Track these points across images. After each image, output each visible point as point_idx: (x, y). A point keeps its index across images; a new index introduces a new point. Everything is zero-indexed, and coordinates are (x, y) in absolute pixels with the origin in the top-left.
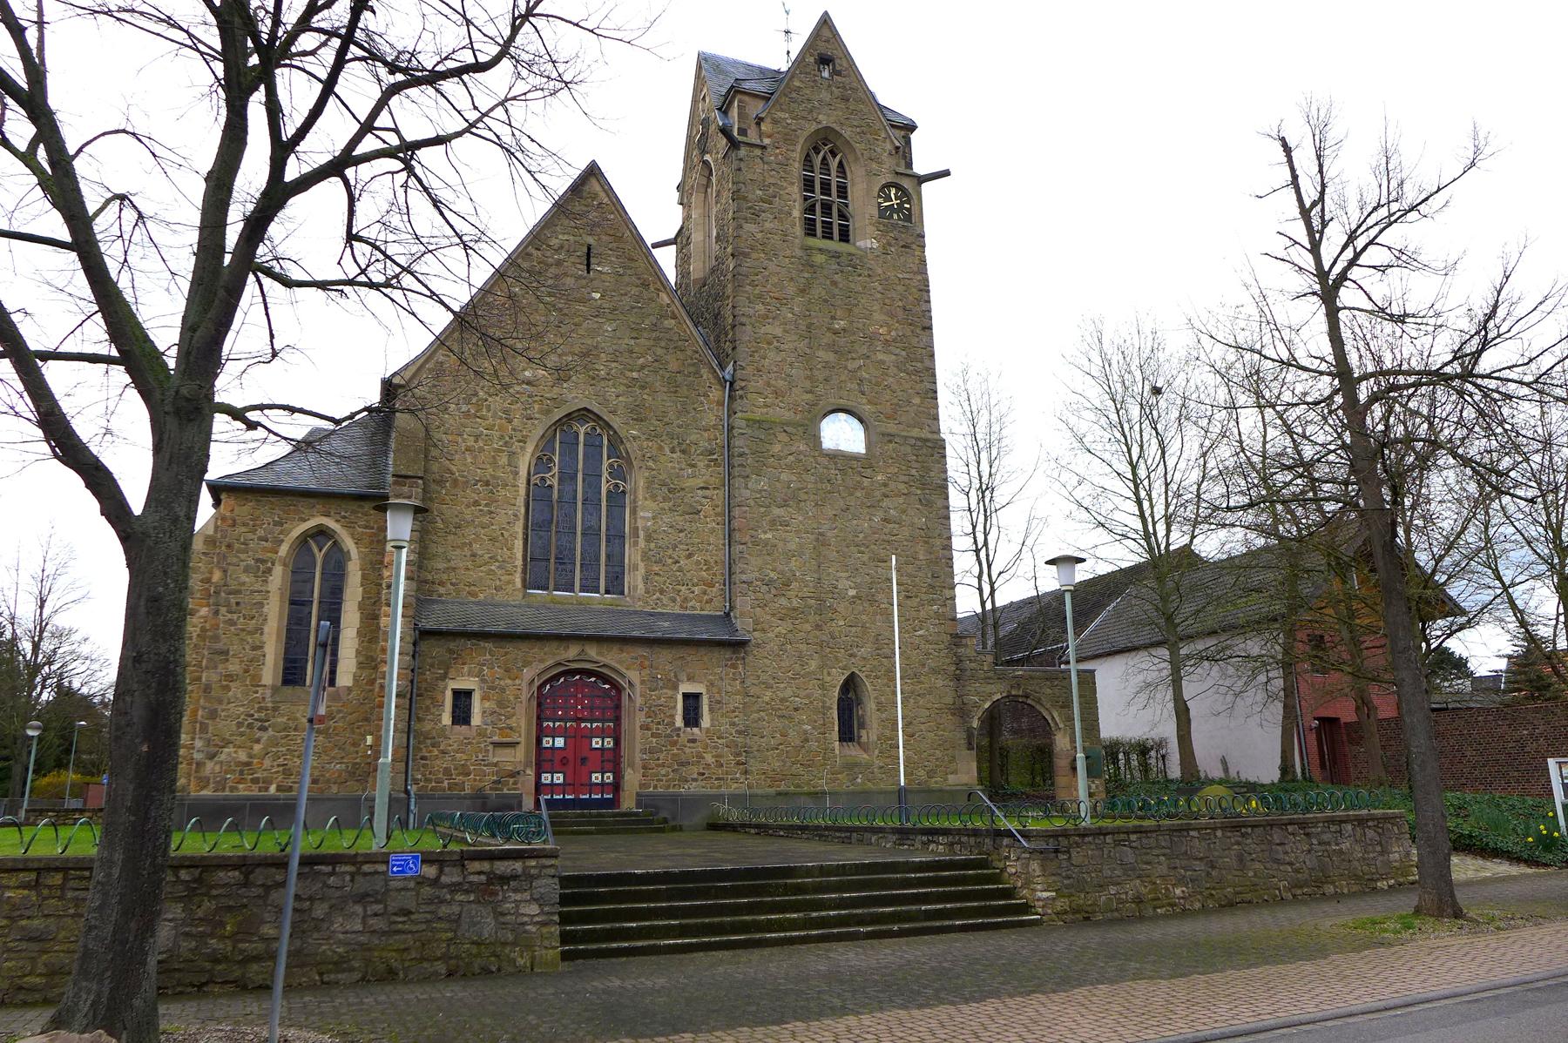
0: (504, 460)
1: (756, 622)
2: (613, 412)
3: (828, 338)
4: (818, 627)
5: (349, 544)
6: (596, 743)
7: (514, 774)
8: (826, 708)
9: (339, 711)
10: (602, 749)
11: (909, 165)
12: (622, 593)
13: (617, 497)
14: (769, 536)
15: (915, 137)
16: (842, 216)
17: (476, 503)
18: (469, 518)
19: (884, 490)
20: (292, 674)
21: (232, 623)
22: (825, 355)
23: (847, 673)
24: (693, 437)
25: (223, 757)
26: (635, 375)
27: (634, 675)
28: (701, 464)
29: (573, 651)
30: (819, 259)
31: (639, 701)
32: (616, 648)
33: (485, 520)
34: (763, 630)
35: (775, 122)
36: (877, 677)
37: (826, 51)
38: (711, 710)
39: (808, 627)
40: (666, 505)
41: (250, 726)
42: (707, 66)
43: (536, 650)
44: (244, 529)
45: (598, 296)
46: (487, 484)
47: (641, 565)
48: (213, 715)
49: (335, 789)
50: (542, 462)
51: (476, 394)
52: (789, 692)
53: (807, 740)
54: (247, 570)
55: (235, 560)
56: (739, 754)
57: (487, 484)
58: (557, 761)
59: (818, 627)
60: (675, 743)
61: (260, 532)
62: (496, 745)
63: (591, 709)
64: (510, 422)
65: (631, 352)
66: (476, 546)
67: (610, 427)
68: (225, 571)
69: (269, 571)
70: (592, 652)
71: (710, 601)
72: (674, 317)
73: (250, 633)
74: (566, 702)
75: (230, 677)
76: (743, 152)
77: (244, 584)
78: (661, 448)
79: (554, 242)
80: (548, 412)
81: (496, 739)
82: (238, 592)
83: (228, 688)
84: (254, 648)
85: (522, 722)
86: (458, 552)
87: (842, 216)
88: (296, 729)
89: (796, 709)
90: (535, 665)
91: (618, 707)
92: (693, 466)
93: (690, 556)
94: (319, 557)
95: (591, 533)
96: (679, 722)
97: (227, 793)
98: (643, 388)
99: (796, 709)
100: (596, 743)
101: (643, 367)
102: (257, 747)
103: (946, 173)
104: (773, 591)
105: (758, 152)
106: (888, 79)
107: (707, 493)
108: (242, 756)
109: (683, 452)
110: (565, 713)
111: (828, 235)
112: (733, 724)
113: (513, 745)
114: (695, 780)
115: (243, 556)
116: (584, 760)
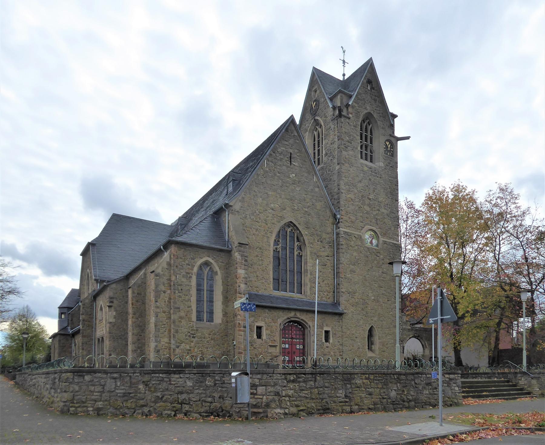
0: (266, 240)
3: (367, 201)
5: (216, 268)
6: (298, 347)
7: (276, 357)
9: (218, 332)
10: (300, 349)
11: (393, 133)
16: (371, 152)
17: (257, 256)
18: (255, 261)
19: (383, 261)
21: (180, 297)
22: (367, 208)
24: (324, 237)
25: (182, 347)
26: (306, 210)
28: (326, 247)
29: (292, 314)
32: (305, 313)
33: (261, 263)
41: (189, 336)
42: (292, 115)
43: (281, 313)
44: (181, 260)
47: (309, 283)
48: (177, 332)
50: (276, 242)
53: (359, 348)
54: (183, 276)
55: (179, 272)
56: (340, 352)
57: (260, 249)
58: (286, 352)
60: (322, 348)
62: (271, 346)
67: (298, 229)
69: (191, 277)
70: (298, 314)
71: (329, 298)
72: (318, 187)
73: (186, 301)
75: (181, 318)
76: (343, 119)
77: (183, 282)
78: (314, 240)
79: (279, 150)
81: (270, 344)
82: (181, 285)
84: (189, 307)
85: (277, 338)
86: (252, 275)
87: (371, 152)
88: (204, 338)
90: (282, 318)
91: (304, 335)
92: (324, 247)
93: (323, 281)
96: (324, 341)
98: (309, 215)
99: (356, 338)
100: (298, 347)
101: (309, 207)
102: (192, 344)
103: (408, 138)
107: (328, 258)
109: (321, 242)
111: (366, 159)
112: (339, 342)
113: (275, 346)
115: (182, 271)
116: (294, 352)
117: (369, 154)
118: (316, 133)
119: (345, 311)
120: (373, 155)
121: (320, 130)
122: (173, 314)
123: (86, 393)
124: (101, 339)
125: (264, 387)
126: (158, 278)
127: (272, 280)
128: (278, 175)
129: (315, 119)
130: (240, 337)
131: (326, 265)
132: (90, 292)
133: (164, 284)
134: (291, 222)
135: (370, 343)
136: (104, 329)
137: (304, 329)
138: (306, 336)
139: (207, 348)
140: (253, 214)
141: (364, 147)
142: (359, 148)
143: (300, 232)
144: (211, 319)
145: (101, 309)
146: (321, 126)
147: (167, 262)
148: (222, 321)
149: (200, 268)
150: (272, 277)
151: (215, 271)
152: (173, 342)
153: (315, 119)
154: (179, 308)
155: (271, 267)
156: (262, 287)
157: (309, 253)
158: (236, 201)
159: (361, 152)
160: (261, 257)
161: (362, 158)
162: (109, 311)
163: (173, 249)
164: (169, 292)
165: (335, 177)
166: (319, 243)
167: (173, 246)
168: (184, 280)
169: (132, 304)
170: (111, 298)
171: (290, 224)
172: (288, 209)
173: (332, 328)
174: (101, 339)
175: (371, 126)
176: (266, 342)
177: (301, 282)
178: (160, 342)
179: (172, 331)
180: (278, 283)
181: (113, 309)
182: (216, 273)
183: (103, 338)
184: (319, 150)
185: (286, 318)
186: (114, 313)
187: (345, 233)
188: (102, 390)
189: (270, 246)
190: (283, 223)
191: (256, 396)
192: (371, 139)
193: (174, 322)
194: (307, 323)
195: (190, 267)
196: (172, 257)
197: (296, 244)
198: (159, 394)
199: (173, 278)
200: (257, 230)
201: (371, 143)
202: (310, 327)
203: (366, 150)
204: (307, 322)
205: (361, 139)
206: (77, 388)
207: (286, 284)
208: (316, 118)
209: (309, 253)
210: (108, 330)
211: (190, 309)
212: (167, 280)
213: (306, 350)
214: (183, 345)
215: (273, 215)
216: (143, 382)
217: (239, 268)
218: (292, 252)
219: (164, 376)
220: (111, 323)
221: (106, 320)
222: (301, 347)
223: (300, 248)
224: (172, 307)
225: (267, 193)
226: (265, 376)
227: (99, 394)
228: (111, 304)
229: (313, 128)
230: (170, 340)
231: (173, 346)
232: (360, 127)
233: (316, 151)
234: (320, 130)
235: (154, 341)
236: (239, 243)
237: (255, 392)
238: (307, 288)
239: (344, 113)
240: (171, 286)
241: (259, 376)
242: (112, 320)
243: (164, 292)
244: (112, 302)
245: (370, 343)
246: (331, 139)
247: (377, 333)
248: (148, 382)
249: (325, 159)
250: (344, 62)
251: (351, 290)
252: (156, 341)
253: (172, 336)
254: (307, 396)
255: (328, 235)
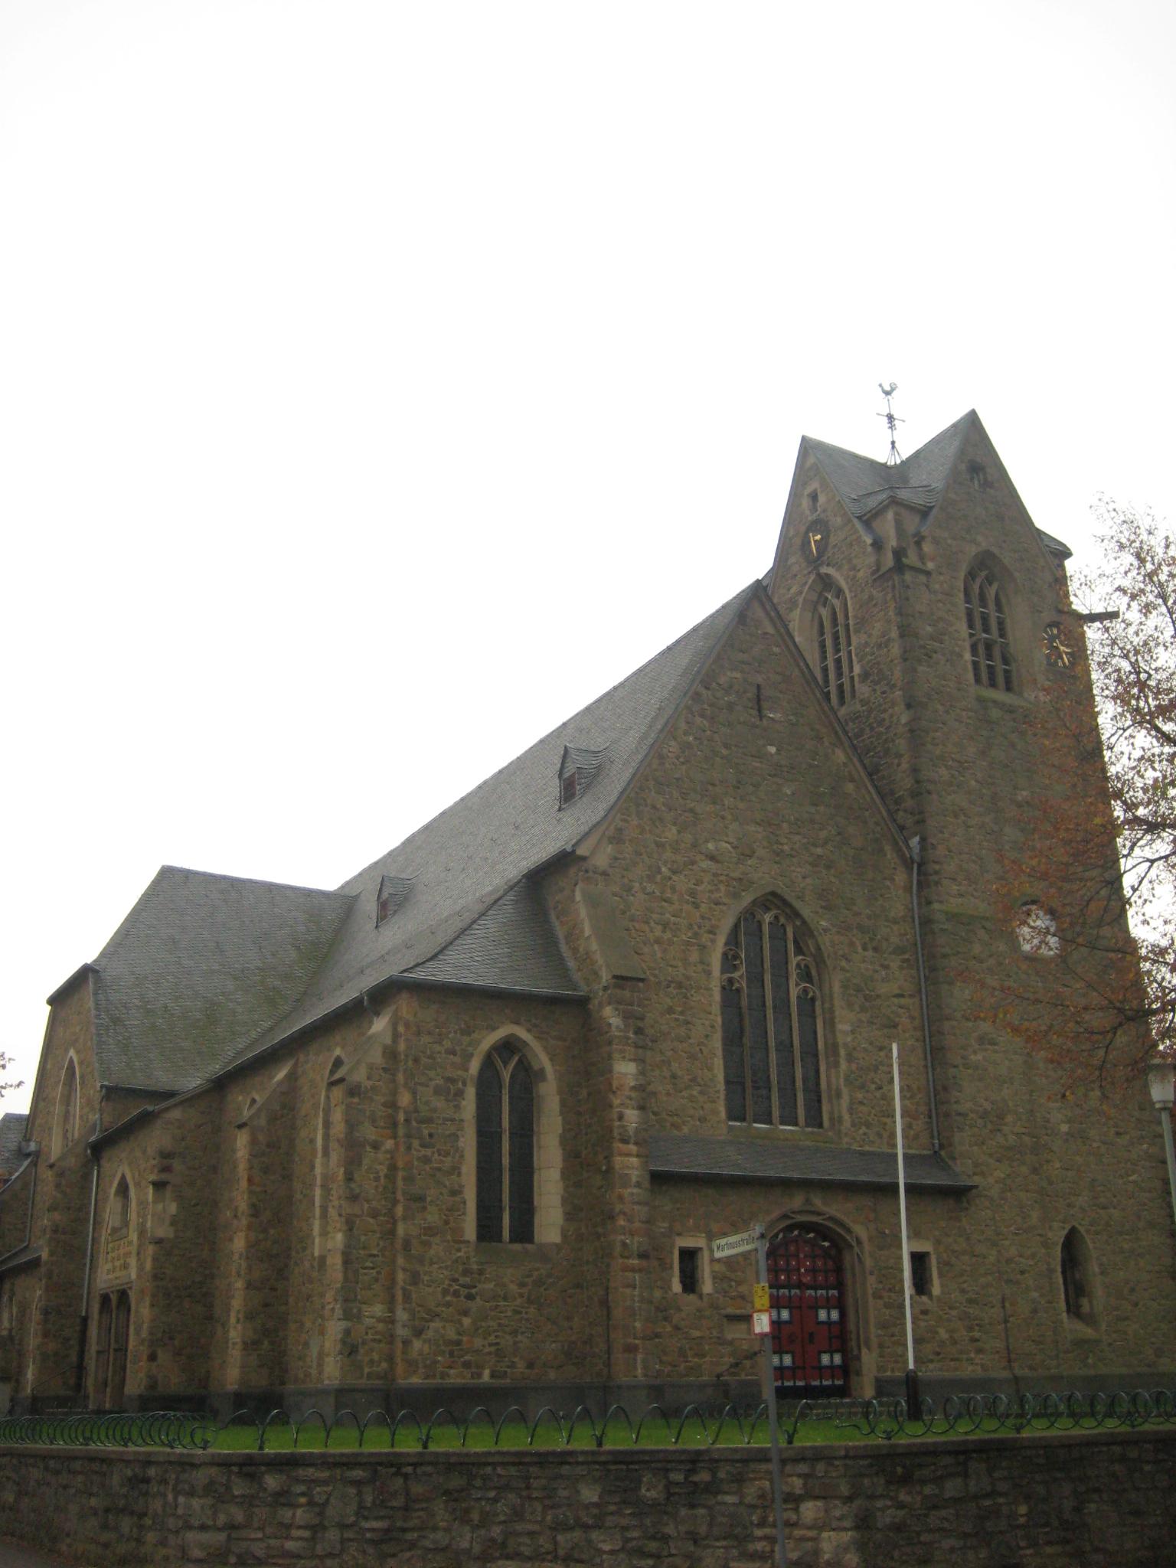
0: (694, 956)
1: (976, 1165)
2: (800, 898)
4: (1035, 1171)
5: (542, 1059)
6: (822, 1315)
8: (1051, 1271)
12: (820, 1125)
13: (808, 1003)
14: (979, 1057)
15: (1069, 565)
16: (1006, 661)
17: (670, 1010)
20: (488, 1230)
21: (426, 1160)
23: (1068, 1227)
25: (430, 1334)
26: (819, 851)
27: (860, 1231)
29: (797, 1201)
30: (995, 713)
31: (869, 1263)
33: (682, 1031)
34: (983, 1174)
35: (936, 541)
36: (1097, 1233)
37: (969, 451)
38: (941, 1275)
39: (1024, 1170)
40: (864, 1017)
41: (456, 1294)
45: (772, 750)
46: (680, 985)
48: (415, 1279)
49: (552, 1375)
50: (729, 961)
51: (660, 872)
52: (1013, 1251)
54: (437, 1091)
56: (970, 1329)
57: (680, 985)
59: (1035, 1171)
61: (447, 1044)
63: (813, 1271)
64: (696, 906)
65: (812, 821)
66: (675, 1065)
68: (414, 1093)
69: (460, 1094)
70: (818, 1202)
72: (852, 780)
74: (788, 1263)
75: (430, 1231)
76: (908, 577)
77: (435, 1110)
80: (736, 896)
81: (730, 1311)
82: (429, 1120)
83: (427, 1244)
88: (505, 1299)
89: (1022, 1273)
91: (839, 1270)
92: (886, 967)
94: (506, 1075)
95: (785, 1047)
97: (889, 1374)
98: (828, 867)
99: (1022, 1273)
102: (467, 1321)
104: (990, 1126)
105: (923, 578)
106: (1053, 498)
107: (903, 1001)
108: (451, 1333)
109: (875, 949)
110: (788, 1277)
111: (993, 684)
112: (963, 1291)
114: (931, 1361)
115: (432, 1074)
117: (1000, 667)
118: (824, 612)
119: (977, 1180)
120: (1013, 667)
121: (836, 603)
122: (404, 1218)
123: (268, 1530)
124: (114, 1298)
125: (819, 1504)
126: (356, 1100)
127: (721, 1087)
128: (725, 752)
129: (819, 575)
130: (628, 1291)
131: (895, 1026)
132: (76, 1129)
133: (373, 1121)
134: (774, 894)
135: (1076, 1290)
136: (133, 1262)
137: (840, 1251)
138: (848, 1275)
139: (514, 1333)
140: (651, 878)
141: (981, 650)
142: (968, 656)
143: (804, 922)
144: (524, 1231)
145: (123, 1190)
146: (839, 592)
147: (385, 1047)
148: (564, 1236)
149: (488, 1062)
150: (721, 1077)
151: (536, 1066)
152: (402, 1315)
153: (819, 575)
154: (421, 1199)
155: (717, 1043)
156: (692, 1112)
157: (837, 988)
158: (600, 841)
159: (975, 664)
160: (682, 1013)
161: (978, 680)
162: (155, 1202)
163: (405, 1006)
164: (389, 1144)
165: (901, 744)
166: (870, 953)
167: (405, 995)
168: (439, 1103)
169: (250, 1180)
170: (165, 1155)
171: (773, 900)
172: (760, 852)
173: (938, 1242)
174: (114, 1298)
175: (995, 586)
176: (714, 1306)
177: (818, 1084)
178: (359, 1317)
179: (400, 1276)
180: (746, 1093)
181: (169, 1192)
182: (541, 1075)
183: (123, 1295)
184: (838, 661)
185: (776, 1214)
186: (173, 1208)
187: (952, 917)
188: (316, 1521)
189: (709, 973)
190: (747, 898)
191: (797, 1533)
192: (1001, 624)
193: (407, 1245)
194: (849, 1230)
195: (457, 1059)
196: (401, 1029)
197: (794, 960)
198: (496, 1531)
199: (405, 1099)
200: (665, 926)
201: (1002, 636)
202: (859, 1242)
203: (989, 657)
204: (847, 1221)
205: (971, 626)
206: (239, 1517)
207: (769, 1098)
208: (824, 570)
209: (837, 988)
210: (148, 1266)
211: (457, 1199)
212: (384, 1105)
213: (852, 1326)
214: (436, 1324)
215: (715, 875)
216: (446, 1492)
217: (616, 1055)
218: (781, 986)
219: (513, 1471)
220: (159, 1242)
221: (142, 1233)
222: (835, 1315)
223: (806, 975)
224: (399, 1196)
225: (692, 810)
226: (820, 1468)
227: (307, 1534)
228: (164, 1177)
229: (814, 597)
230: (391, 1310)
231: (401, 1332)
232: (962, 595)
233: (830, 663)
234: (836, 603)
235: (339, 1313)
236: (615, 977)
237: (794, 1517)
238: (840, 1106)
239: (912, 559)
240: (395, 1125)
241: (803, 1468)
242: (164, 1231)
243: (376, 1146)
244: (166, 1169)
245: (1076, 1290)
246: (875, 633)
247: (1092, 1247)
248: (462, 1490)
249: (863, 690)
250: (890, 417)
251: (987, 1106)
252: (347, 1316)
253: (399, 1297)
254: (946, 1525)
255: (895, 928)
